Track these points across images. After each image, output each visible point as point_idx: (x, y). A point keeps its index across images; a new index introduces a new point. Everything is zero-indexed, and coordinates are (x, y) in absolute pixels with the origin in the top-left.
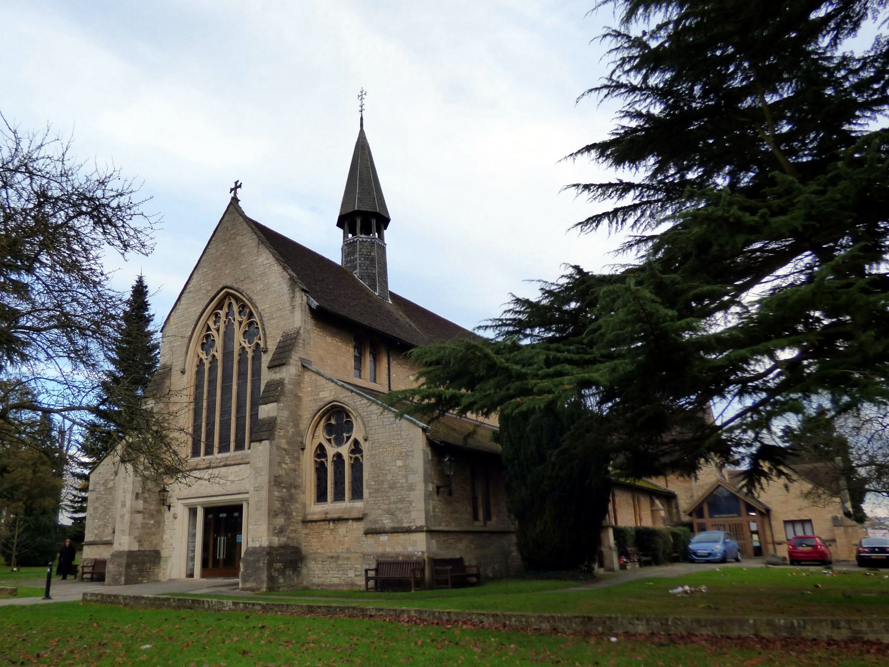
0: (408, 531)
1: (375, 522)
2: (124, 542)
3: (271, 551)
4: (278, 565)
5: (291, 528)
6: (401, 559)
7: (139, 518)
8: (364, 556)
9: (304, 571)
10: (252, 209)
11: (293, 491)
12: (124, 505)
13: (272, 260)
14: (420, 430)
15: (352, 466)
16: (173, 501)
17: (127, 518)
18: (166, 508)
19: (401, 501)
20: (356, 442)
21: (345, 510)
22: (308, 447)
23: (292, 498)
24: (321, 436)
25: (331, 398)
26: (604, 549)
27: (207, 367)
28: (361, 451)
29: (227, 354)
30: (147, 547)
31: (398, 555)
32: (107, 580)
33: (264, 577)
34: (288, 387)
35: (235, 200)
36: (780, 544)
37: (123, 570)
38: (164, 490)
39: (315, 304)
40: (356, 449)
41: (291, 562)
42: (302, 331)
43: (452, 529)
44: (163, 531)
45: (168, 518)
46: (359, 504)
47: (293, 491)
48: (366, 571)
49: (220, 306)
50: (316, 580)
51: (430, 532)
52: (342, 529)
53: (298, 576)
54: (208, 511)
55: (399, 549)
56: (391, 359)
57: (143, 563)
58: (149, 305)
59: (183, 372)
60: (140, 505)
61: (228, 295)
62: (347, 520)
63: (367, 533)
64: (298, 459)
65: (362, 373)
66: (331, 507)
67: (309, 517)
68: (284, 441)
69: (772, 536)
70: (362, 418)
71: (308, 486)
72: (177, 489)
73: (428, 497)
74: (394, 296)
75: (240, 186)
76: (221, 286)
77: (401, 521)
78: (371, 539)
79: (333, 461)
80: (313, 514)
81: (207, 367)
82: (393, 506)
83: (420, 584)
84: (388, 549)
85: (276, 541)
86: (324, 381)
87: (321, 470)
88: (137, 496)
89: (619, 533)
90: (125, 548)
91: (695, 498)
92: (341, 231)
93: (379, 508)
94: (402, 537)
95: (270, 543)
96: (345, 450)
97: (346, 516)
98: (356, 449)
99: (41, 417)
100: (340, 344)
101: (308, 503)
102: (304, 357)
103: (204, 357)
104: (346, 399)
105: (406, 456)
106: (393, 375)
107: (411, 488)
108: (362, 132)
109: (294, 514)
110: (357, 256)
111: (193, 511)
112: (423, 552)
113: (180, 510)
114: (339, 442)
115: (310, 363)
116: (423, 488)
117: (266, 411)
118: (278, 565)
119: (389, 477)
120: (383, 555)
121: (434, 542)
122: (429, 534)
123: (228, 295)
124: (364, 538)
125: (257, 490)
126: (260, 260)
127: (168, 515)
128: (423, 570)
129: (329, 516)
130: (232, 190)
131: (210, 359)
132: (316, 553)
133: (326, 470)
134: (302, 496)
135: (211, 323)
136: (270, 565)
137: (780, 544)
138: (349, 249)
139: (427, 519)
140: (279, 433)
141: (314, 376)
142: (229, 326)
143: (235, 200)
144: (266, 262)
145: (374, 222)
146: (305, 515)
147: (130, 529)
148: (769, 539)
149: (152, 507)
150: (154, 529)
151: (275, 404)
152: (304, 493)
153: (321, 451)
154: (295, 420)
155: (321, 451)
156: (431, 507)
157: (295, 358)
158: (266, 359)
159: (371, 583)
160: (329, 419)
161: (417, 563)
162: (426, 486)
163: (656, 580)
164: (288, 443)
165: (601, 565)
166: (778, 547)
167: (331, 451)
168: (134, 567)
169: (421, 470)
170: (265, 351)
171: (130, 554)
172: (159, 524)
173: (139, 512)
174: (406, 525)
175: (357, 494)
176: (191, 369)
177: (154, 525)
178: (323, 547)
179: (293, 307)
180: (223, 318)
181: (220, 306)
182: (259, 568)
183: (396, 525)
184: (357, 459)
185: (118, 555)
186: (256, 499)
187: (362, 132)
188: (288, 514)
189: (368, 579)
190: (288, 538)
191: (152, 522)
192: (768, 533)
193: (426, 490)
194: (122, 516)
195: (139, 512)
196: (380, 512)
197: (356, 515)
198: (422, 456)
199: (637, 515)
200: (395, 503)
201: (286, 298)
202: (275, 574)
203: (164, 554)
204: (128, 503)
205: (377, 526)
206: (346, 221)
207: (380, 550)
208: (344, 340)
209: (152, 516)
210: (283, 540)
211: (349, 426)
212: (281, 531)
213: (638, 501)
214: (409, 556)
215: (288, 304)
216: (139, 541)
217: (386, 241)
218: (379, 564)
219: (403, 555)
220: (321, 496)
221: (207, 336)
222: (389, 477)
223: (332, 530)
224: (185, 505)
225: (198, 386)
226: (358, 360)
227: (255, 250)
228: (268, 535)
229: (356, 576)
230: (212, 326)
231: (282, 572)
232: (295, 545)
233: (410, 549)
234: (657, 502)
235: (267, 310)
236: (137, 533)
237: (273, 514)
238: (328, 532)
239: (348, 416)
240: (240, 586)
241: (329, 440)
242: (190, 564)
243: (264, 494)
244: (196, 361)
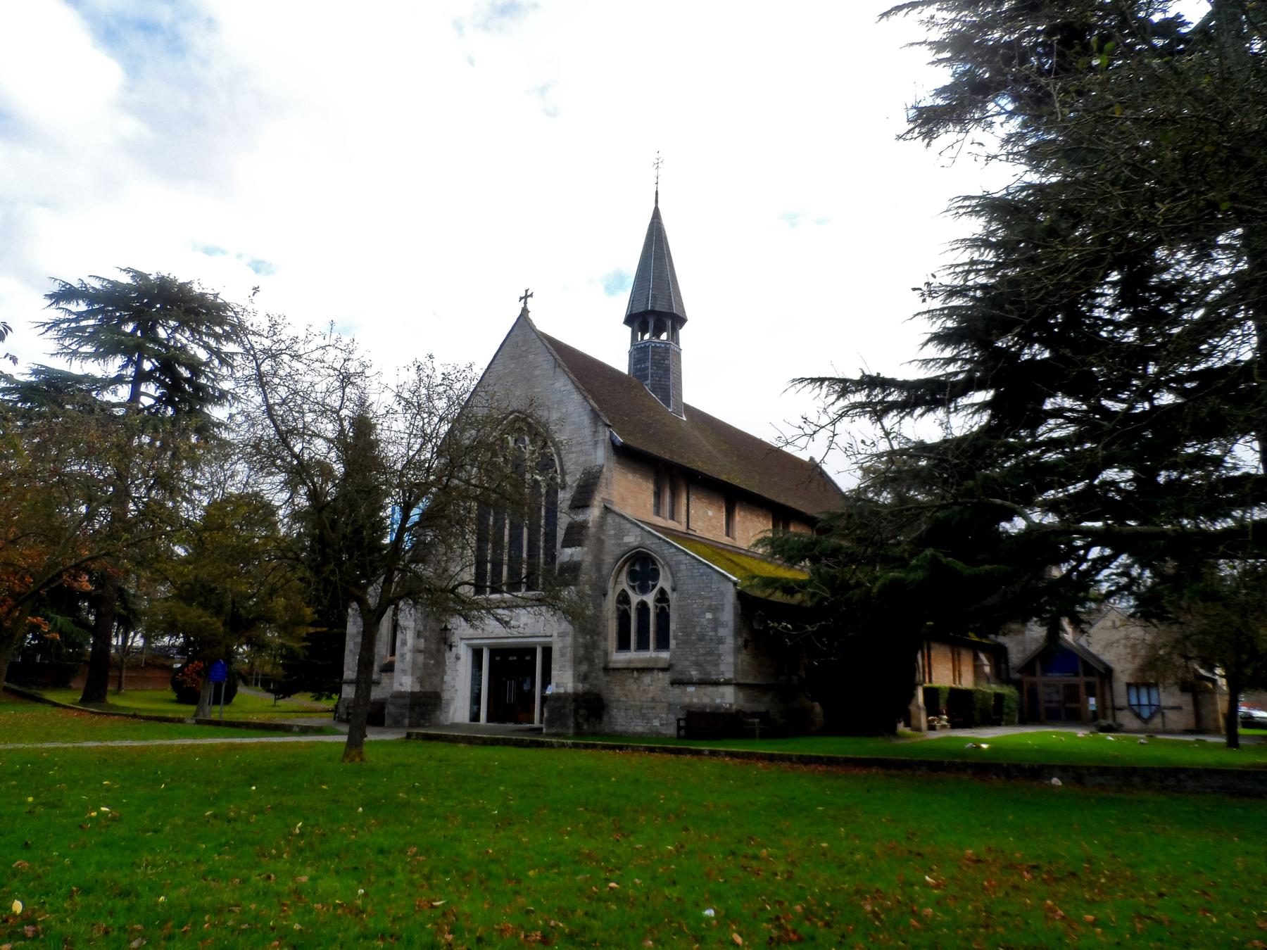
0: (716, 683)
1: (682, 673)
2: (405, 682)
3: (576, 697)
5: (594, 675)
6: (708, 710)
7: (421, 658)
8: (670, 707)
9: (605, 718)
10: (544, 323)
11: (595, 637)
13: (570, 387)
14: (732, 585)
15: (658, 616)
16: (455, 639)
17: (409, 657)
18: (447, 648)
19: (710, 653)
20: (662, 591)
21: (650, 660)
22: (610, 592)
23: (594, 645)
24: (624, 583)
25: (636, 544)
26: (912, 708)
28: (667, 601)
30: (428, 689)
32: (387, 722)
33: (571, 723)
34: (592, 529)
35: (525, 311)
36: (1121, 709)
38: (446, 629)
40: (662, 597)
42: (604, 470)
44: (444, 673)
45: (449, 658)
46: (665, 655)
47: (595, 637)
48: (678, 720)
51: (739, 686)
52: (647, 679)
53: (600, 723)
54: (494, 652)
55: (706, 700)
56: (691, 499)
58: (216, 296)
60: (422, 643)
63: (674, 683)
64: (600, 605)
65: (661, 511)
66: (633, 656)
67: (611, 665)
68: (587, 587)
69: (1112, 700)
70: (670, 567)
71: (610, 633)
72: (460, 629)
73: (737, 651)
74: (690, 411)
75: (531, 295)
78: (677, 691)
79: (637, 608)
80: (617, 662)
82: (701, 658)
84: (695, 700)
86: (629, 526)
87: (623, 619)
89: (932, 694)
91: (1028, 653)
92: (628, 330)
93: (687, 659)
94: (710, 689)
96: (650, 598)
98: (662, 597)
99: (287, 535)
100: (640, 481)
101: (610, 650)
102: (607, 497)
104: (654, 546)
105: (715, 609)
106: (692, 511)
107: (721, 641)
108: (656, 215)
109: (597, 661)
110: (649, 364)
111: (477, 653)
112: (731, 705)
114: (644, 590)
115: (611, 502)
116: (732, 642)
117: (567, 554)
118: (582, 712)
119: (698, 629)
121: (741, 694)
124: (670, 688)
126: (557, 385)
127: (449, 656)
129: (632, 665)
130: (521, 299)
132: (619, 701)
133: (629, 618)
134: (603, 643)
137: (1121, 709)
138: (639, 354)
139: (735, 673)
140: (583, 578)
141: (618, 519)
143: (525, 311)
144: (563, 388)
145: (669, 323)
146: (607, 662)
147: (413, 669)
148: (1109, 704)
150: (434, 670)
151: (579, 549)
152: (606, 639)
153: (624, 599)
154: (598, 564)
155: (624, 599)
156: (739, 661)
157: (597, 500)
158: (564, 497)
159: (682, 732)
160: (633, 565)
162: (736, 641)
163: (956, 739)
164: (591, 588)
165: (908, 724)
166: (1118, 713)
167: (635, 599)
169: (731, 624)
170: (564, 487)
173: (420, 651)
174: (714, 677)
175: (663, 643)
177: (434, 665)
178: (626, 696)
179: (596, 443)
183: (703, 677)
184: (663, 609)
186: (561, 645)
187: (656, 215)
189: (679, 728)
190: (591, 685)
191: (432, 662)
192: (1108, 697)
193: (735, 643)
195: (420, 651)
196: (687, 663)
198: (732, 610)
199: (957, 672)
200: (704, 655)
201: (587, 432)
202: (581, 720)
205: (684, 677)
206: (636, 320)
207: (687, 700)
208: (645, 476)
210: (587, 686)
211: (655, 575)
213: (959, 657)
214: (719, 707)
216: (421, 682)
217: (682, 345)
219: (710, 707)
220: (623, 645)
222: (698, 629)
223: (636, 679)
224: (468, 645)
226: (658, 495)
227: (551, 373)
228: (574, 682)
229: (662, 725)
231: (587, 719)
233: (718, 701)
234: (982, 656)
237: (577, 661)
238: (632, 681)
239: (655, 564)
240: (544, 730)
241: (633, 588)
242: (475, 708)
243: (569, 640)
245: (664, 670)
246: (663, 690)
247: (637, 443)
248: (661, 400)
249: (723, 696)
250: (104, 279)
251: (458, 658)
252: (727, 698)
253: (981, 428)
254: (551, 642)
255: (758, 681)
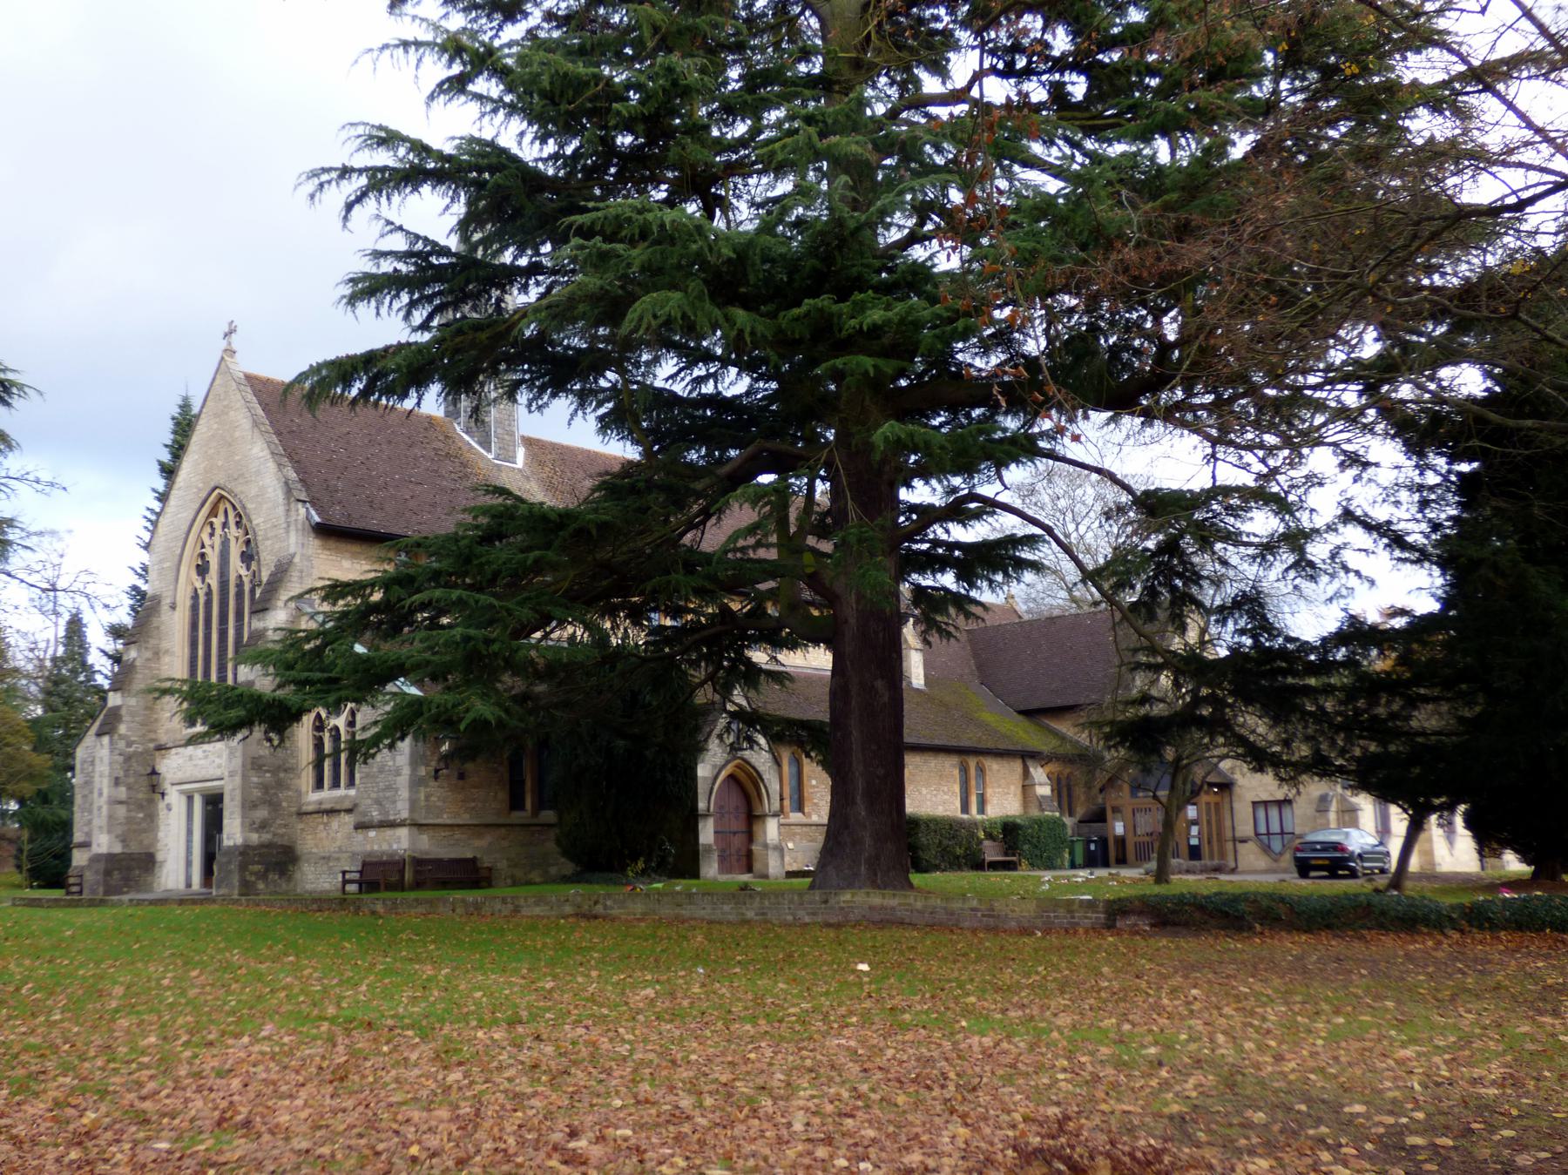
0: (393, 825)
2: (103, 843)
4: (257, 868)
7: (122, 811)
9: (298, 875)
11: (282, 775)
12: (101, 794)
19: (389, 788)
27: (202, 600)
29: (224, 584)
30: (134, 848)
31: (383, 853)
33: (236, 880)
37: (100, 877)
38: (154, 773)
39: (317, 519)
41: (277, 864)
42: (297, 560)
43: (460, 822)
46: (352, 792)
49: (213, 512)
50: (309, 887)
52: (335, 823)
57: (129, 869)
59: (173, 607)
60: (122, 792)
61: (222, 497)
62: (338, 811)
66: (327, 795)
67: (305, 808)
76: (213, 484)
77: (387, 813)
78: (359, 836)
80: (309, 804)
81: (202, 600)
83: (399, 886)
85: (255, 838)
88: (117, 782)
90: (104, 850)
94: (389, 832)
95: (245, 840)
97: (338, 807)
101: (304, 789)
103: (198, 584)
111: (190, 799)
113: (174, 798)
120: (370, 854)
122: (415, 829)
123: (222, 497)
125: (232, 774)
127: (162, 805)
128: (402, 872)
129: (324, 807)
131: (205, 589)
135: (205, 537)
136: (243, 867)
137: (1244, 841)
142: (225, 543)
148: (1229, 834)
149: (140, 796)
150: (144, 825)
161: (396, 863)
166: (1240, 846)
168: (116, 875)
171: (110, 858)
172: (152, 818)
173: (121, 803)
176: (184, 603)
177: (143, 819)
180: (219, 531)
181: (213, 512)
182: (230, 872)
185: (96, 859)
188: (274, 806)
194: (100, 808)
195: (121, 803)
197: (347, 805)
203: (160, 857)
204: (105, 792)
205: (366, 819)
209: (140, 807)
210: (266, 837)
212: (263, 826)
215: (283, 519)
216: (123, 841)
218: (364, 864)
220: (319, 784)
221: (203, 555)
223: (326, 824)
224: (182, 792)
225: (194, 626)
228: (243, 832)
230: (207, 542)
231: (263, 876)
232: (285, 843)
233: (395, 847)
235: (262, 527)
236: (119, 830)
244: (190, 593)
245: (349, 811)
246: (349, 837)
247: (338, 517)
248: (480, 444)
249: (398, 840)
250: (418, 237)
251: (169, 808)
252: (400, 842)
253: (1456, 364)
254: (222, 787)
255: (465, 818)
